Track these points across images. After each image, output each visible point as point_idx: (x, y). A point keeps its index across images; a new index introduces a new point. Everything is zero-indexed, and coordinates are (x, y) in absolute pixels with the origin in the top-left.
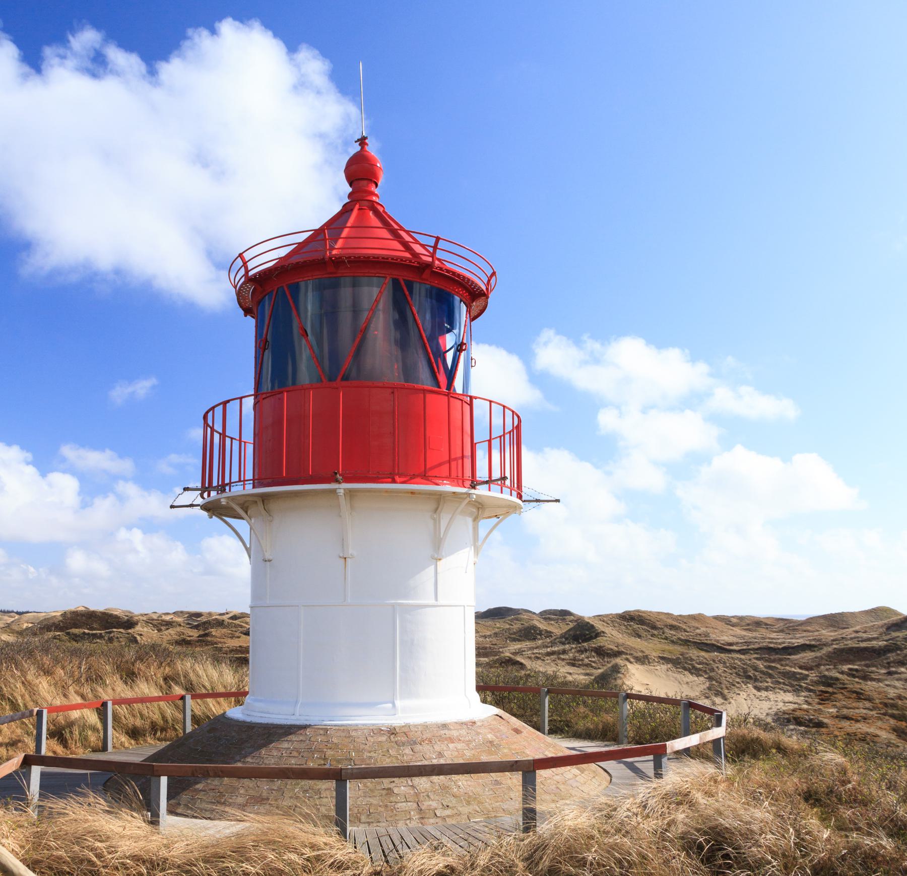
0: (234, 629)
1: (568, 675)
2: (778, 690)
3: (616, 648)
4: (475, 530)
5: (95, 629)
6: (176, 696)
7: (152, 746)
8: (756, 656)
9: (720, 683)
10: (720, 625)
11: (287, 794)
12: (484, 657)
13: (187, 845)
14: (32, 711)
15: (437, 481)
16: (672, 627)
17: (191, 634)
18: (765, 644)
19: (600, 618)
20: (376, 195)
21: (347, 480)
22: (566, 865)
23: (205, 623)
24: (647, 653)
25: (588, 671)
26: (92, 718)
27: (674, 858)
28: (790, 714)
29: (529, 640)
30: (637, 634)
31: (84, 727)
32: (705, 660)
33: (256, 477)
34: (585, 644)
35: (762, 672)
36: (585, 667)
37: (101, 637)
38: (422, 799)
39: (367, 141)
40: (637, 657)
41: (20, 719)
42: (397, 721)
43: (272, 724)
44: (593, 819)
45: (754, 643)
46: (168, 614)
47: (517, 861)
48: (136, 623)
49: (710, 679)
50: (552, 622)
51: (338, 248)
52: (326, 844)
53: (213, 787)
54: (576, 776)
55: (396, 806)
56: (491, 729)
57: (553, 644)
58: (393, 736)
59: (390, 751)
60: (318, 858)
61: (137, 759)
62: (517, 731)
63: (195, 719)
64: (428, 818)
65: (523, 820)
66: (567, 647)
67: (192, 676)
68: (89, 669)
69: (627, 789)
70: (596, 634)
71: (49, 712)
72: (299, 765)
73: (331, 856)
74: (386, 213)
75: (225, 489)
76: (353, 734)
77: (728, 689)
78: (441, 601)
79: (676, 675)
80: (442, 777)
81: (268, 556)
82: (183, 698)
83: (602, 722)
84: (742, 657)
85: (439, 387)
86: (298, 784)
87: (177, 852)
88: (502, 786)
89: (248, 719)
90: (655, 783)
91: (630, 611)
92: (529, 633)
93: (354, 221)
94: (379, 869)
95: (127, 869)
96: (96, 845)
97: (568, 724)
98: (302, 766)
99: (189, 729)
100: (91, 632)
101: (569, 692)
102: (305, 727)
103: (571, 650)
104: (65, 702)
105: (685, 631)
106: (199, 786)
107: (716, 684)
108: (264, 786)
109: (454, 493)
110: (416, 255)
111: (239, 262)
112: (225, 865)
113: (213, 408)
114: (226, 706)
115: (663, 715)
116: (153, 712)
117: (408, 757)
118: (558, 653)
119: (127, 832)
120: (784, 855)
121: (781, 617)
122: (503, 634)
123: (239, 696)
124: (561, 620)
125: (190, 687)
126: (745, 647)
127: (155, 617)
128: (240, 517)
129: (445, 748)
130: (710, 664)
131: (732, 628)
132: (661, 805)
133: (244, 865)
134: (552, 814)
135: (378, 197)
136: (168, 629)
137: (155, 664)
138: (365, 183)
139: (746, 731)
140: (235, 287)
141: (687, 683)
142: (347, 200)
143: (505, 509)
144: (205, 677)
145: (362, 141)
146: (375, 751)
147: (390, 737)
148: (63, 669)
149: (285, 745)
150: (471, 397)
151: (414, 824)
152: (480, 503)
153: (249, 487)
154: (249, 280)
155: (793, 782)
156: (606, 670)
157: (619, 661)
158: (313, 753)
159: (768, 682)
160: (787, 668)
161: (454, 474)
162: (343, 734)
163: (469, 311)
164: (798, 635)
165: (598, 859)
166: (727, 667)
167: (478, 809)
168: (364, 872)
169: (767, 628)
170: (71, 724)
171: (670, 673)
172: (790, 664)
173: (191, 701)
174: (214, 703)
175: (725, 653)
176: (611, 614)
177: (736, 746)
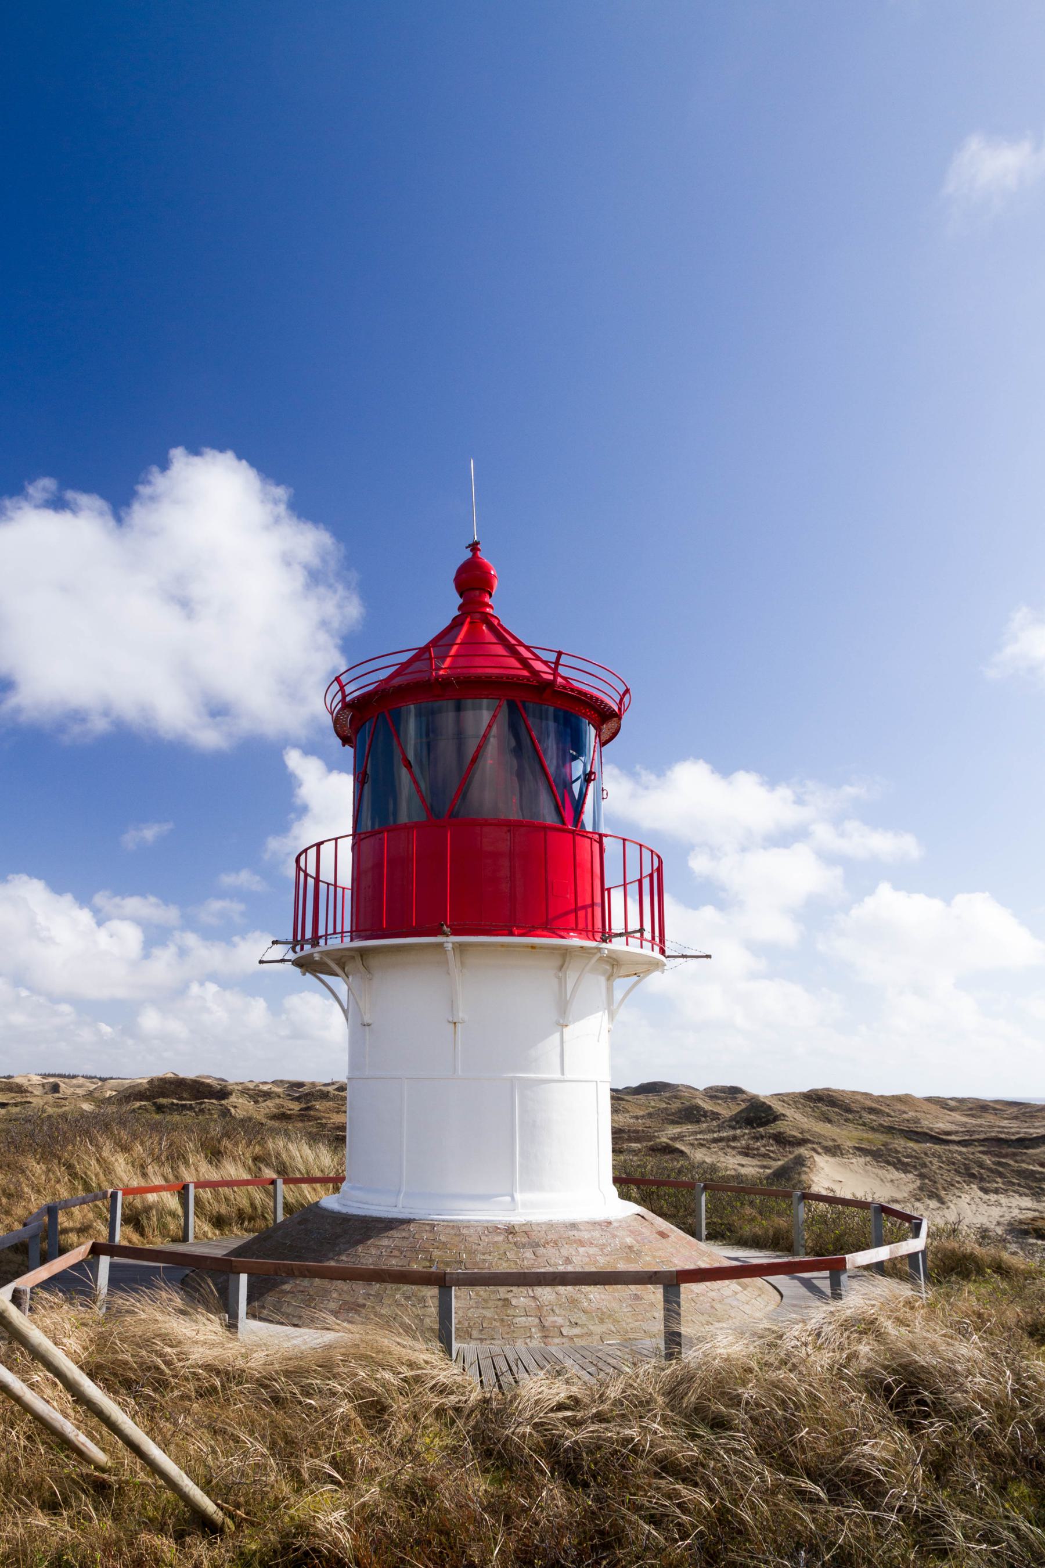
0: (341, 1103)
1: (740, 1168)
2: (1011, 1193)
3: (800, 1135)
4: (610, 990)
5: (184, 1099)
6: (267, 1179)
7: (238, 1237)
8: (981, 1149)
9: (935, 1182)
10: (934, 1109)
11: (387, 1301)
12: (635, 1143)
13: (267, 1356)
14: (107, 1192)
15: (562, 933)
16: (872, 1110)
17: (292, 1107)
18: (993, 1134)
19: (780, 1097)
20: (491, 607)
21: (456, 933)
22: (716, 1403)
23: (307, 1094)
24: (839, 1142)
25: (765, 1163)
26: (172, 1202)
27: (853, 1401)
28: (1028, 1224)
29: (692, 1122)
30: (827, 1118)
31: (164, 1212)
32: (913, 1153)
33: (354, 929)
34: (761, 1129)
35: (989, 1169)
36: (761, 1158)
37: (190, 1108)
38: (544, 1313)
39: (479, 546)
40: (827, 1147)
41: (93, 1201)
42: (517, 1218)
43: (371, 1217)
44: (752, 1348)
45: (979, 1132)
46: (266, 1083)
47: (655, 1395)
48: (231, 1094)
49: (922, 1176)
50: (720, 1102)
51: (444, 668)
52: (426, 1362)
53: (302, 1289)
54: (736, 1293)
55: (514, 1321)
56: (630, 1231)
57: (721, 1128)
58: (512, 1235)
59: (508, 1254)
60: (417, 1379)
61: (219, 1253)
62: (663, 1235)
63: (288, 1208)
64: (552, 1337)
65: (666, 1344)
66: (738, 1132)
67: (284, 1156)
68: (171, 1145)
69: (795, 1312)
70: (777, 1118)
71: (124, 1194)
72: (402, 1266)
73: (433, 1378)
74: (501, 626)
75: (318, 943)
76: (465, 1231)
77: (946, 1190)
78: (568, 1076)
79: (876, 1171)
80: (569, 1288)
81: (367, 1019)
82: (273, 1182)
83: (772, 1226)
84: (964, 1150)
85: (564, 823)
86: (399, 1289)
87: (257, 1362)
88: (643, 1301)
89: (344, 1210)
90: (833, 1306)
91: (817, 1090)
92: (691, 1114)
93: (465, 636)
94: (488, 1395)
95: (199, 1380)
96: (165, 1350)
97: (730, 1228)
98: (403, 1269)
99: (280, 1218)
100: (180, 1102)
101: (731, 1189)
102: (409, 1221)
103: (743, 1136)
104: (143, 1184)
105: (889, 1115)
106: (287, 1287)
107: (930, 1183)
108: (360, 1289)
109: (582, 947)
110: (535, 673)
111: (336, 687)
112: (309, 1381)
113: (306, 851)
114: (323, 1193)
115: (856, 1218)
116: (241, 1198)
117: (528, 1262)
118: (728, 1139)
119: (201, 1337)
120: (998, 1405)
121: (1014, 1100)
122: (659, 1115)
123: (336, 1181)
124: (731, 1098)
125: (282, 1170)
126: (967, 1138)
127: (251, 1086)
128: (333, 974)
129: (574, 1253)
130: (922, 1158)
131: (949, 1113)
132: (838, 1334)
133: (330, 1382)
134: (701, 1340)
135: (493, 608)
136: (265, 1101)
137: (244, 1142)
138: (477, 593)
139: (956, 1245)
140: (332, 713)
141: (892, 1181)
142: (458, 613)
143: (645, 966)
144: (299, 1159)
145: (474, 547)
146: (490, 1253)
147: (507, 1237)
148: (142, 1145)
149: (385, 1242)
150: (601, 836)
151: (536, 1343)
152: (614, 960)
153: (347, 939)
154: (346, 705)
155: (1014, 1312)
156: (788, 1162)
157: (802, 1151)
158: (417, 1252)
159: (997, 1183)
160: (1024, 1165)
161: (581, 926)
162: (453, 1232)
163: (598, 734)
164: (1037, 1124)
165: (756, 1399)
166: (943, 1162)
167: (613, 1329)
168: (471, 1399)
169: (996, 1114)
170: (148, 1209)
171: (869, 1168)
172: (1028, 1160)
173: (283, 1186)
174: (310, 1189)
175: (940, 1144)
176: (793, 1093)
177: (944, 1263)
